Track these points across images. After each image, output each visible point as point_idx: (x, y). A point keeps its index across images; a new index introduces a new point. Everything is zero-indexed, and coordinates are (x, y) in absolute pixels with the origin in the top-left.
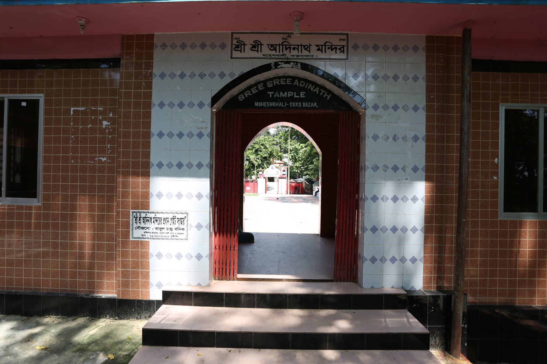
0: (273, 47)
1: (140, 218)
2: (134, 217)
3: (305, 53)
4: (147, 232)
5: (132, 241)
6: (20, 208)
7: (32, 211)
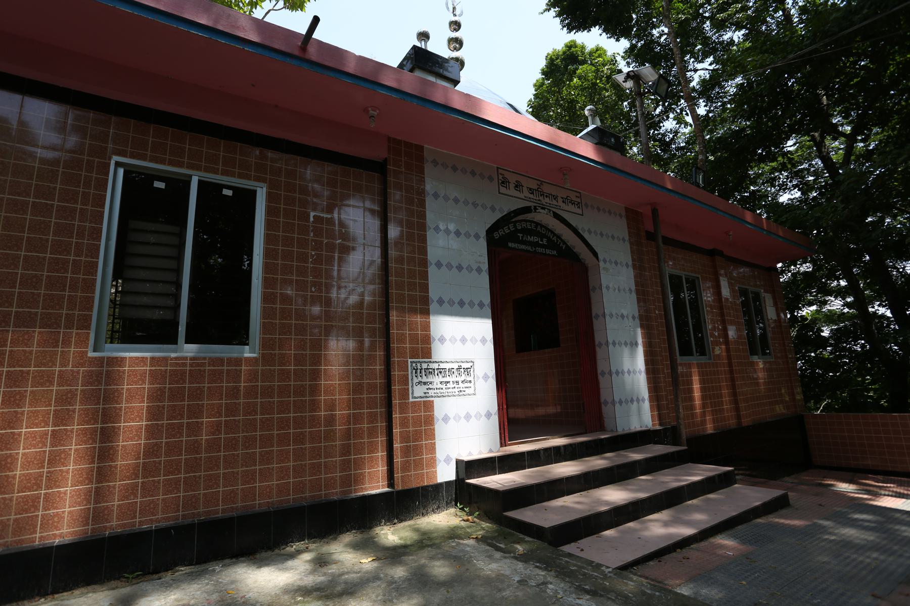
0: (531, 191)
1: (420, 370)
2: (414, 369)
3: (554, 202)
4: (430, 389)
5: (412, 402)
6: (220, 361)
7: (241, 366)
